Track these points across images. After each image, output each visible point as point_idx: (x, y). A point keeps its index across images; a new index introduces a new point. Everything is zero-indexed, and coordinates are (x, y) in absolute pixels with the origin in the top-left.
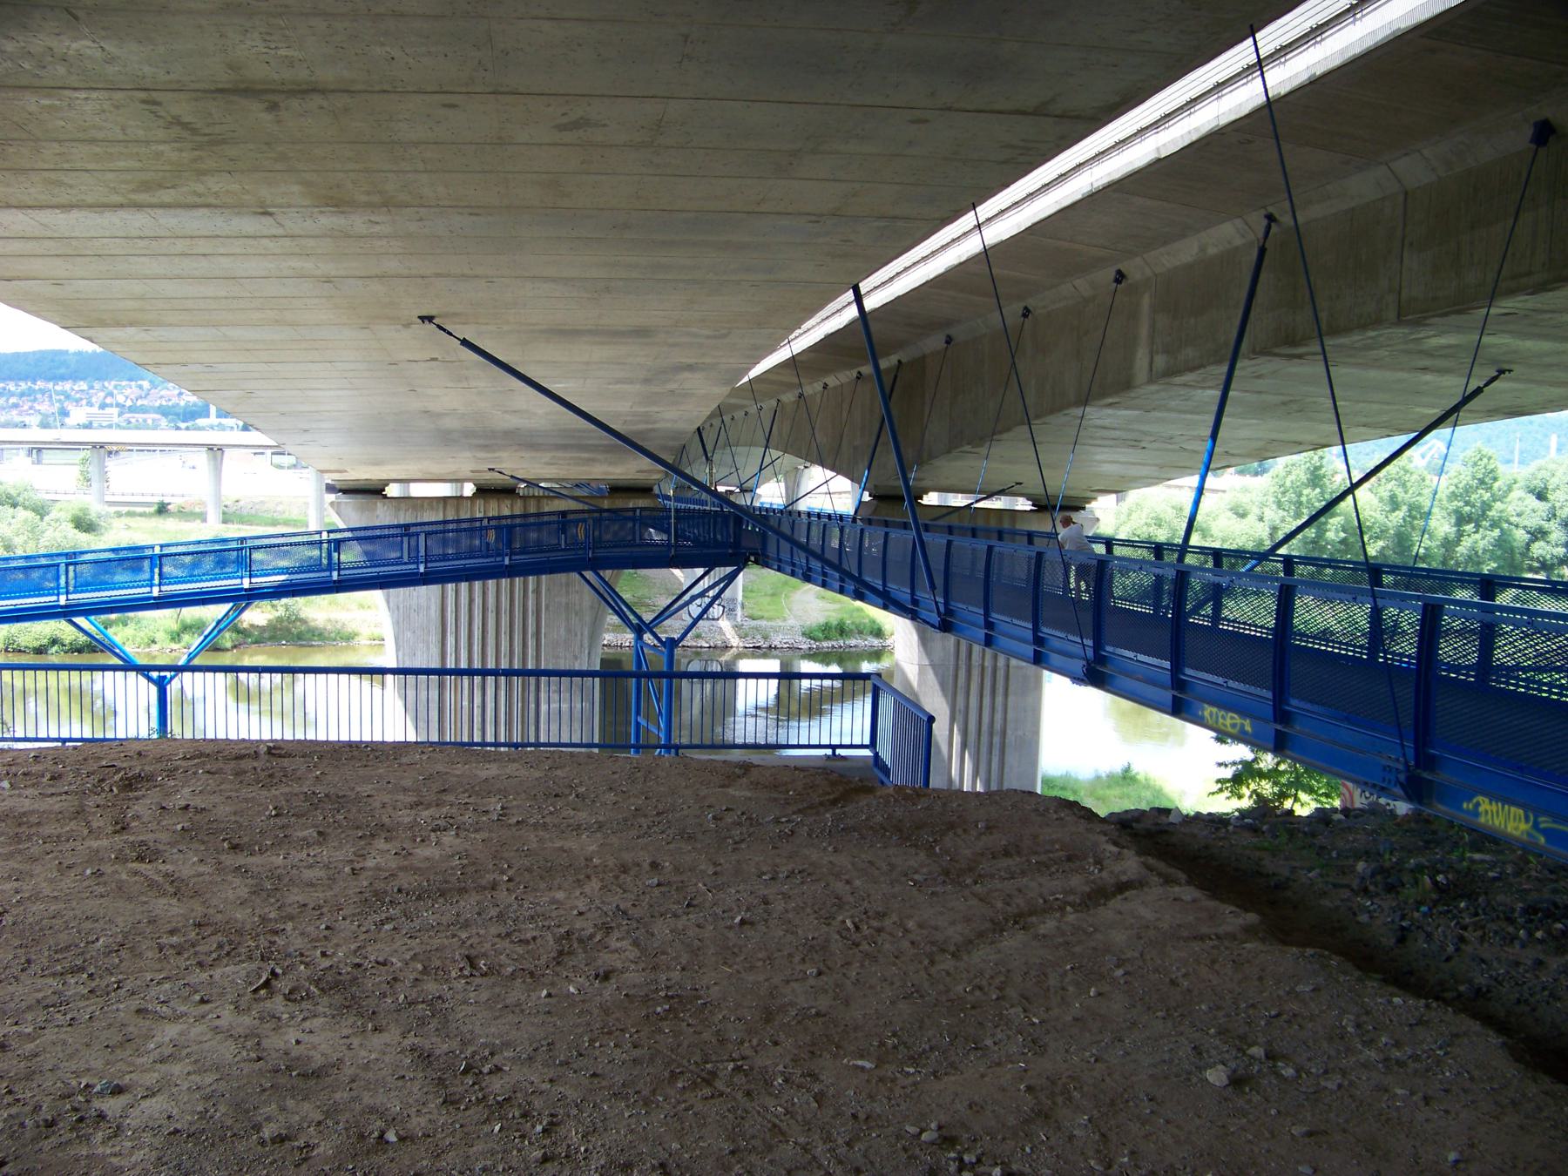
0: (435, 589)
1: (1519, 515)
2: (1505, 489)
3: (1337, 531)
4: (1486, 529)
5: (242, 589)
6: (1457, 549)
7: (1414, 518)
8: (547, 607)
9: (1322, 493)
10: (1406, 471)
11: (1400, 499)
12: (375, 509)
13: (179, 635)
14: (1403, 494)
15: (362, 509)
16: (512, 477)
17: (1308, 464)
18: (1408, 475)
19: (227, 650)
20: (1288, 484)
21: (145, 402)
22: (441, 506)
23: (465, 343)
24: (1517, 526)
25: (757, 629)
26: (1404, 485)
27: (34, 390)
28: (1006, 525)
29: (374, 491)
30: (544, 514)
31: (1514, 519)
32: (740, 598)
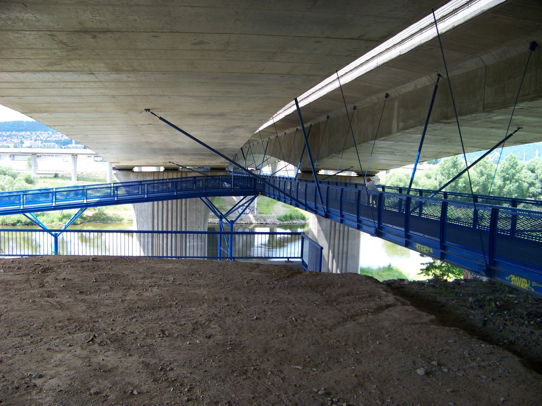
0: (150, 203)
1: (525, 178)
2: (520, 169)
3: (462, 183)
4: (514, 183)
5: (84, 203)
6: (504, 190)
7: (489, 179)
8: (189, 210)
9: (457, 170)
10: (486, 163)
11: (484, 172)
12: (130, 176)
13: (62, 219)
14: (485, 171)
15: (125, 176)
16: (177, 165)
17: (452, 160)
18: (487, 164)
19: (79, 224)
20: (445, 167)
21: (50, 139)
22: (152, 175)
23: (161, 118)
24: (524, 182)
25: (262, 217)
26: (485, 167)
27: (12, 135)
28: (348, 181)
29: (129, 170)
30: (188, 177)
31: (523, 179)
32: (256, 207)
